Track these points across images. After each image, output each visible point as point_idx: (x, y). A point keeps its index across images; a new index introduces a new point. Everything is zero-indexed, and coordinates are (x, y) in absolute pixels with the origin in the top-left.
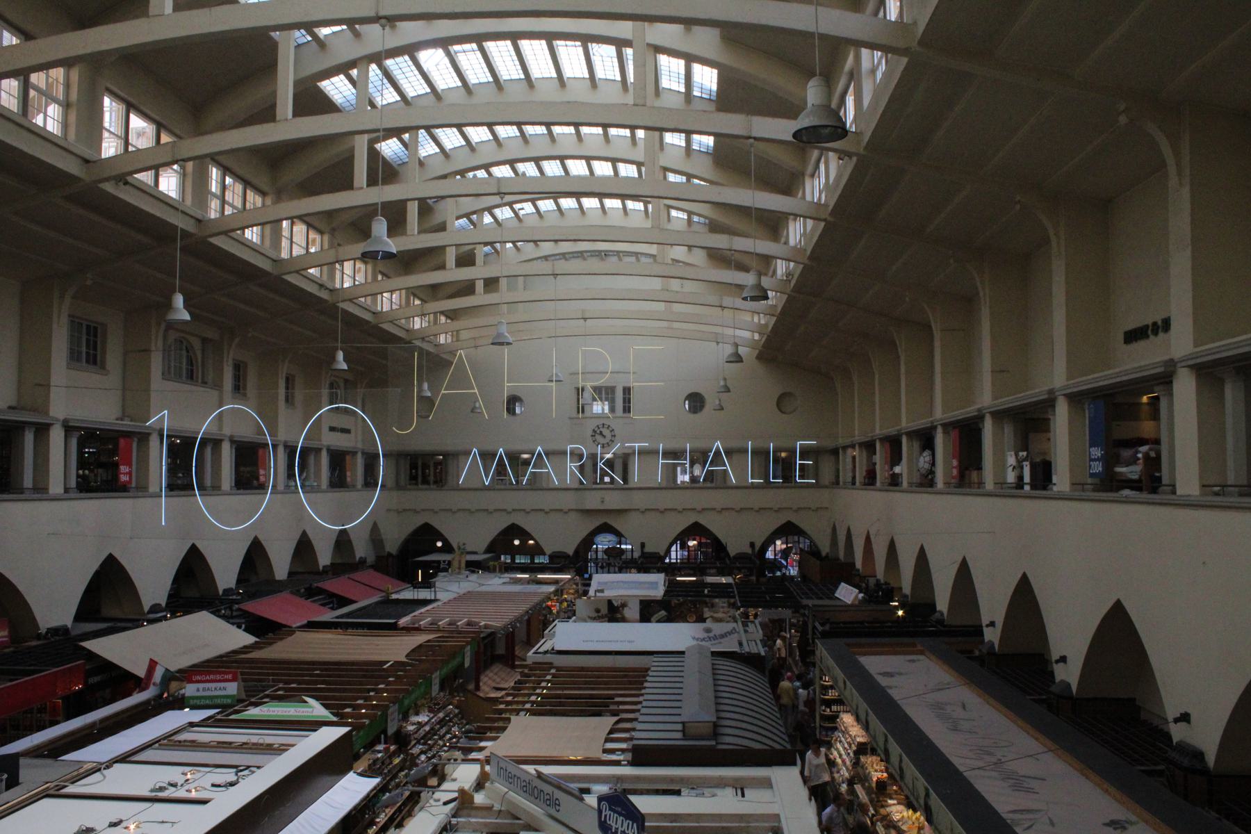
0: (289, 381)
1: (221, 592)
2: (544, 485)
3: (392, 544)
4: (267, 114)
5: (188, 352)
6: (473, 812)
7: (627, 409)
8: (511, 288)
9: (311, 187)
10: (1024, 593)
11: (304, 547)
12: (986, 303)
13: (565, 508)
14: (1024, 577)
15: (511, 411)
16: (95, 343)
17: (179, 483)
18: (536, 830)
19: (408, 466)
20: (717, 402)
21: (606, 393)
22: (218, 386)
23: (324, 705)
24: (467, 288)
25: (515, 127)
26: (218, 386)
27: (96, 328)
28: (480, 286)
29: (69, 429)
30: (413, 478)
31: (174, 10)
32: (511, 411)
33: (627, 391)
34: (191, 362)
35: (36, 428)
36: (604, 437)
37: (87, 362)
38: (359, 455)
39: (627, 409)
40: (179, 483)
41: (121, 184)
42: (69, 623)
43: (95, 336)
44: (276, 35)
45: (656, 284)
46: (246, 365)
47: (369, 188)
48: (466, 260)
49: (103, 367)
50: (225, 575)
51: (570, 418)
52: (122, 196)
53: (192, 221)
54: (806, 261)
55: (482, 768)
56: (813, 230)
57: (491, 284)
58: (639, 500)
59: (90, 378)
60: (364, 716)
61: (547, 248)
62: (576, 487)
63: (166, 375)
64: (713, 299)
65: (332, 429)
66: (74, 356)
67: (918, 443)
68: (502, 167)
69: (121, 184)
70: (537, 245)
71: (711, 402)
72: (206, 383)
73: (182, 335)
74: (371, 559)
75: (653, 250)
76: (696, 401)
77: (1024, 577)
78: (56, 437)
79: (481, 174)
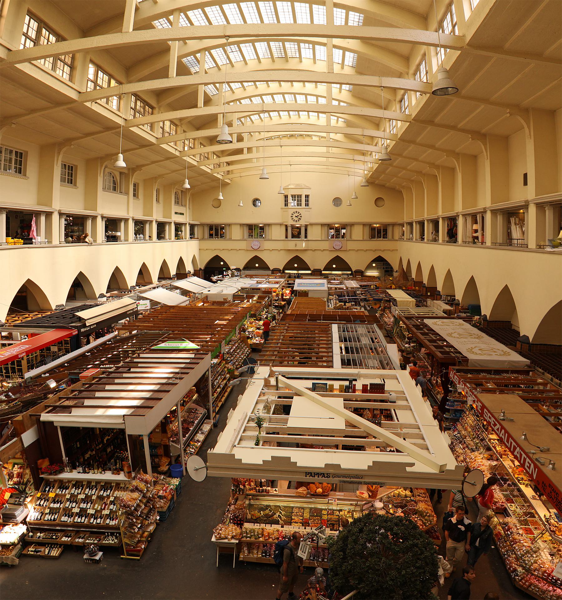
0: (158, 191)
1: (129, 288)
2: (270, 238)
3: (201, 265)
4: (164, 73)
5: (113, 178)
6: (270, 388)
7: (307, 205)
8: (258, 151)
9: (173, 107)
10: (472, 283)
11: (164, 267)
12: (488, 159)
13: (279, 249)
14: (472, 277)
15: (254, 205)
16: (72, 173)
17: (111, 239)
18: (299, 395)
19: (209, 229)
20: (349, 202)
21: (297, 198)
22: (127, 193)
23: (463, 321)
24: (239, 151)
25: (239, 84)
26: (127, 193)
27: (72, 167)
28: (245, 151)
29: (61, 214)
30: (211, 236)
31: (133, 30)
32: (254, 205)
33: (307, 196)
34: (114, 183)
35: (46, 214)
36: (296, 216)
37: (68, 182)
38: (188, 225)
39: (307, 205)
40: (161, 236)
41: (94, 103)
42: (64, 302)
43: (72, 171)
44: (170, 43)
45: (324, 149)
46: (138, 184)
47: (205, 107)
48: (240, 139)
49: (75, 185)
50: (131, 279)
51: (282, 209)
52: (93, 108)
53: (123, 120)
54: (398, 140)
55: (271, 368)
56: (401, 127)
57: (249, 150)
58: (313, 245)
59: (69, 189)
60: (210, 346)
61: (263, 135)
62: (283, 239)
63: (104, 189)
64: (350, 157)
65: (176, 213)
66: (63, 180)
67: (501, 216)
68: (246, 100)
69: (94, 103)
70: (260, 134)
71: (345, 202)
72: (122, 193)
73: (111, 170)
74: (192, 272)
75: (324, 135)
76: (337, 202)
77: (472, 277)
78: (55, 217)
79: (247, 101)
